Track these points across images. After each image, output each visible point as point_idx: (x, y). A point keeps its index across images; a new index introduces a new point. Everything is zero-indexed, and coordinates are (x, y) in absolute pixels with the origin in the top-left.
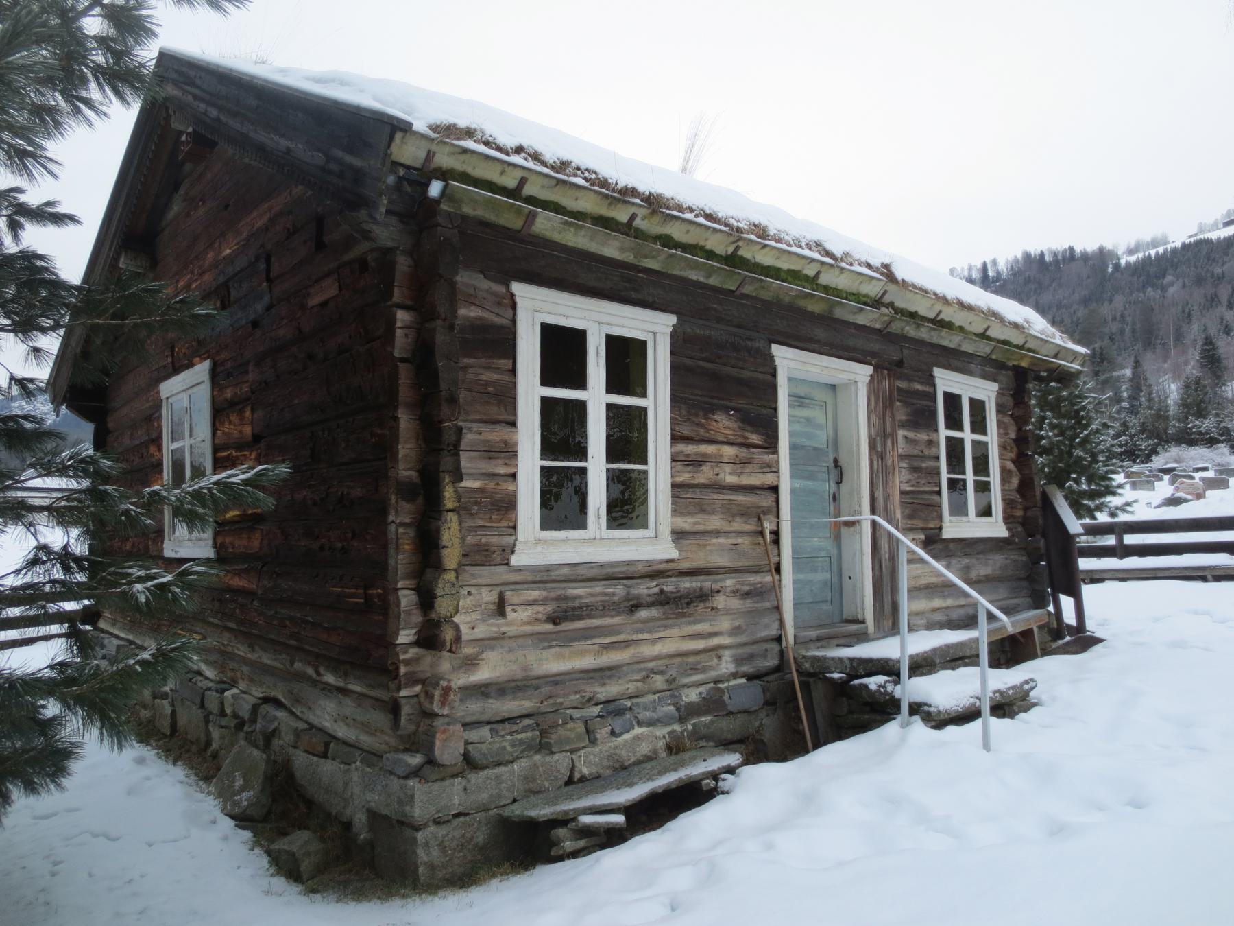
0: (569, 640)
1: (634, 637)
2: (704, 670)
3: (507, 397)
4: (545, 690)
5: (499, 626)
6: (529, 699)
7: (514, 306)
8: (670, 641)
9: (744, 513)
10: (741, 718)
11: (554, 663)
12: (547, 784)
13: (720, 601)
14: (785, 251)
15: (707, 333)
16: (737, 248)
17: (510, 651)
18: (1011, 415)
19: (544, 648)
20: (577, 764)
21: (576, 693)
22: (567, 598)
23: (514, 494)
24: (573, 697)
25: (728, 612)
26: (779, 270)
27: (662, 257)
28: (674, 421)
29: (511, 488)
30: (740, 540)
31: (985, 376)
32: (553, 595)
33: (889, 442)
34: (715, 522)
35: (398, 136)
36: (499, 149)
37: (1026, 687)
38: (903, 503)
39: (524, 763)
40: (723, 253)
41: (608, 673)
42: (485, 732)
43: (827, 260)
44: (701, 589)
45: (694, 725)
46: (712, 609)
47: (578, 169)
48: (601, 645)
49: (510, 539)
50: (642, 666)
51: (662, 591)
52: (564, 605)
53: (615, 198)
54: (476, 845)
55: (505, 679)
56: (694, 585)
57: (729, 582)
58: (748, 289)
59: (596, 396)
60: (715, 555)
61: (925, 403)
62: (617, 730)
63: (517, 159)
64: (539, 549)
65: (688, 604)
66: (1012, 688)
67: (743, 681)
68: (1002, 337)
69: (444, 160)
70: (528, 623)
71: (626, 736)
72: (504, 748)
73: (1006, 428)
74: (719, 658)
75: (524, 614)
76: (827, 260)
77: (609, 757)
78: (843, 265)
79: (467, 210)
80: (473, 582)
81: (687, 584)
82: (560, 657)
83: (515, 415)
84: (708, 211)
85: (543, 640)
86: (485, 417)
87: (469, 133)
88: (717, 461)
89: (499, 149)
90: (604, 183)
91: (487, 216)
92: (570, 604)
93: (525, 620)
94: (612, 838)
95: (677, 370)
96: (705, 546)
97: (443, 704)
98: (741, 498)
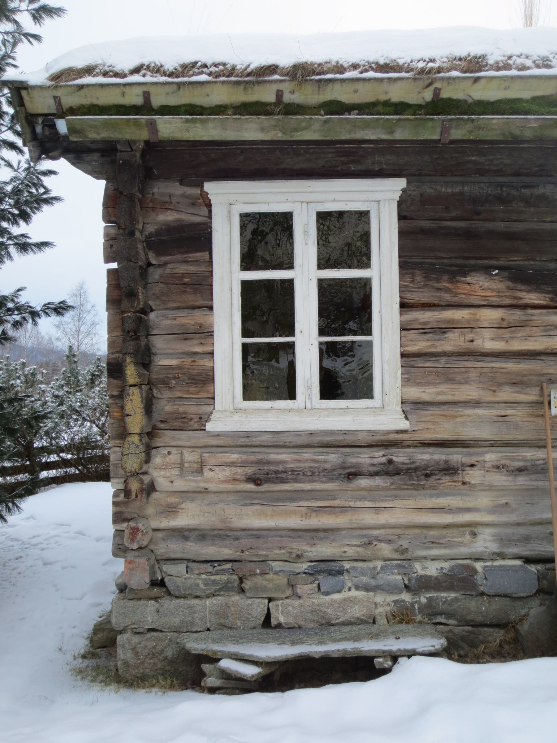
0: (272, 500)
1: (352, 504)
3: (203, 285)
4: (245, 542)
5: (196, 481)
7: (209, 205)
8: (403, 511)
9: (518, 382)
10: (497, 605)
11: (254, 518)
12: (239, 623)
13: (474, 476)
14: (512, 78)
15: (457, 189)
16: (437, 92)
17: (209, 504)
20: (273, 611)
21: (281, 548)
22: (269, 463)
23: (213, 369)
24: (277, 552)
25: (490, 488)
27: (316, 126)
28: (403, 289)
29: (208, 364)
30: (510, 412)
32: (253, 458)
35: (24, 93)
36: (116, 75)
39: (216, 601)
40: (420, 102)
41: (322, 534)
42: (181, 568)
44: (446, 462)
45: (430, 599)
46: (464, 483)
47: (205, 66)
49: (208, 409)
50: (365, 532)
51: (390, 462)
52: (266, 468)
53: (247, 82)
54: (166, 658)
55: (209, 527)
56: (436, 457)
57: (491, 457)
58: (457, 134)
59: (306, 276)
60: (471, 426)
62: (323, 589)
63: (136, 78)
64: (236, 417)
65: (427, 476)
67: (518, 562)
69: (69, 101)
70: (227, 482)
71: (336, 596)
72: (198, 585)
74: (474, 535)
75: (224, 473)
77: (313, 612)
79: (92, 135)
80: (173, 443)
81: (424, 456)
83: (212, 300)
84: (382, 62)
85: (246, 499)
86: (182, 305)
87: (89, 70)
88: (472, 327)
89: (116, 75)
90: (232, 71)
91: (112, 136)
92: (273, 468)
93: (222, 478)
94: (238, 686)
96: (454, 417)
97: (133, 540)
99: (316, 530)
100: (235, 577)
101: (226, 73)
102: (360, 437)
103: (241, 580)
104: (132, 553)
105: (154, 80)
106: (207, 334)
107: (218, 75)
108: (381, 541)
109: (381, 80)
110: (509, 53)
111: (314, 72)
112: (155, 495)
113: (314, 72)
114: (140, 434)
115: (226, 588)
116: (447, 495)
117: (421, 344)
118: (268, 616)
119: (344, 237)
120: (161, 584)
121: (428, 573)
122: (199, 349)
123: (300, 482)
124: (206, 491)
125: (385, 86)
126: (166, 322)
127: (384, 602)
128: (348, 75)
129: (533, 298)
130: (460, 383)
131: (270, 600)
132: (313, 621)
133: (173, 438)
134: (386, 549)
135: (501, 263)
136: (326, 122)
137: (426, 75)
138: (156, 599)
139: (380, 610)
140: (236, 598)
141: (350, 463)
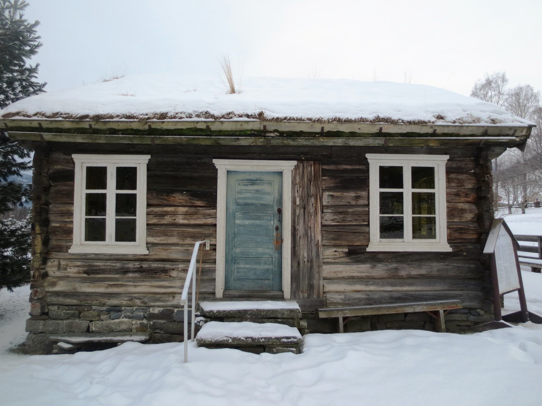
1: (125, 283)
2: (162, 301)
3: (70, 195)
6: (75, 299)
7: (74, 163)
8: (145, 287)
12: (76, 330)
15: (171, 159)
16: (150, 126)
18: (474, 173)
19: (84, 283)
20: (90, 326)
21: (96, 301)
22: (94, 266)
24: (95, 302)
26: (182, 129)
28: (148, 199)
31: (431, 151)
32: (87, 264)
33: (312, 200)
34: (174, 240)
36: (28, 116)
37: (285, 340)
38: (322, 230)
42: (56, 308)
43: (210, 120)
44: (163, 267)
45: (154, 323)
46: (170, 276)
47: (62, 114)
48: (108, 284)
49: (70, 244)
50: (131, 295)
51: (141, 267)
52: (92, 268)
54: (46, 344)
56: (160, 265)
58: (157, 142)
59: (111, 192)
61: (354, 175)
65: (156, 273)
66: (265, 338)
68: (404, 132)
69: (10, 124)
71: (117, 321)
73: (461, 183)
74: (174, 297)
75: (75, 270)
76: (210, 120)
77: (106, 326)
78: (222, 120)
80: (56, 257)
81: (155, 265)
82: (89, 286)
85: (83, 280)
88: (175, 214)
89: (28, 116)
90: (71, 117)
92: (95, 268)
94: (71, 351)
95: (150, 177)
96: (167, 250)
98: (191, 230)
99: (112, 294)
100: (77, 312)
101: (68, 117)
102: (130, 257)
103: (80, 313)
104: (35, 301)
105: (42, 119)
106: (70, 214)
107: (66, 118)
108: (137, 299)
109: (127, 122)
110: (177, 112)
111: (102, 118)
112: (48, 278)
113: (102, 118)
114: (40, 253)
115: (73, 316)
116: (163, 281)
117: (154, 221)
118: (89, 327)
119: (127, 177)
120: (47, 314)
121: (154, 312)
122: (68, 220)
123: (105, 274)
124: (69, 277)
125: (129, 124)
126: (55, 209)
127: (136, 323)
128: (115, 119)
129: (199, 203)
130: (170, 236)
131: (91, 321)
132: (106, 330)
133: (56, 255)
134: (138, 302)
135: (185, 189)
136: (106, 137)
137: (145, 120)
138: (44, 320)
139: (134, 326)
140: (77, 320)
141: (123, 267)
